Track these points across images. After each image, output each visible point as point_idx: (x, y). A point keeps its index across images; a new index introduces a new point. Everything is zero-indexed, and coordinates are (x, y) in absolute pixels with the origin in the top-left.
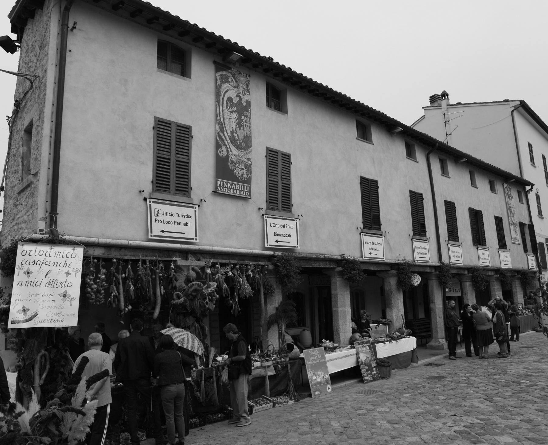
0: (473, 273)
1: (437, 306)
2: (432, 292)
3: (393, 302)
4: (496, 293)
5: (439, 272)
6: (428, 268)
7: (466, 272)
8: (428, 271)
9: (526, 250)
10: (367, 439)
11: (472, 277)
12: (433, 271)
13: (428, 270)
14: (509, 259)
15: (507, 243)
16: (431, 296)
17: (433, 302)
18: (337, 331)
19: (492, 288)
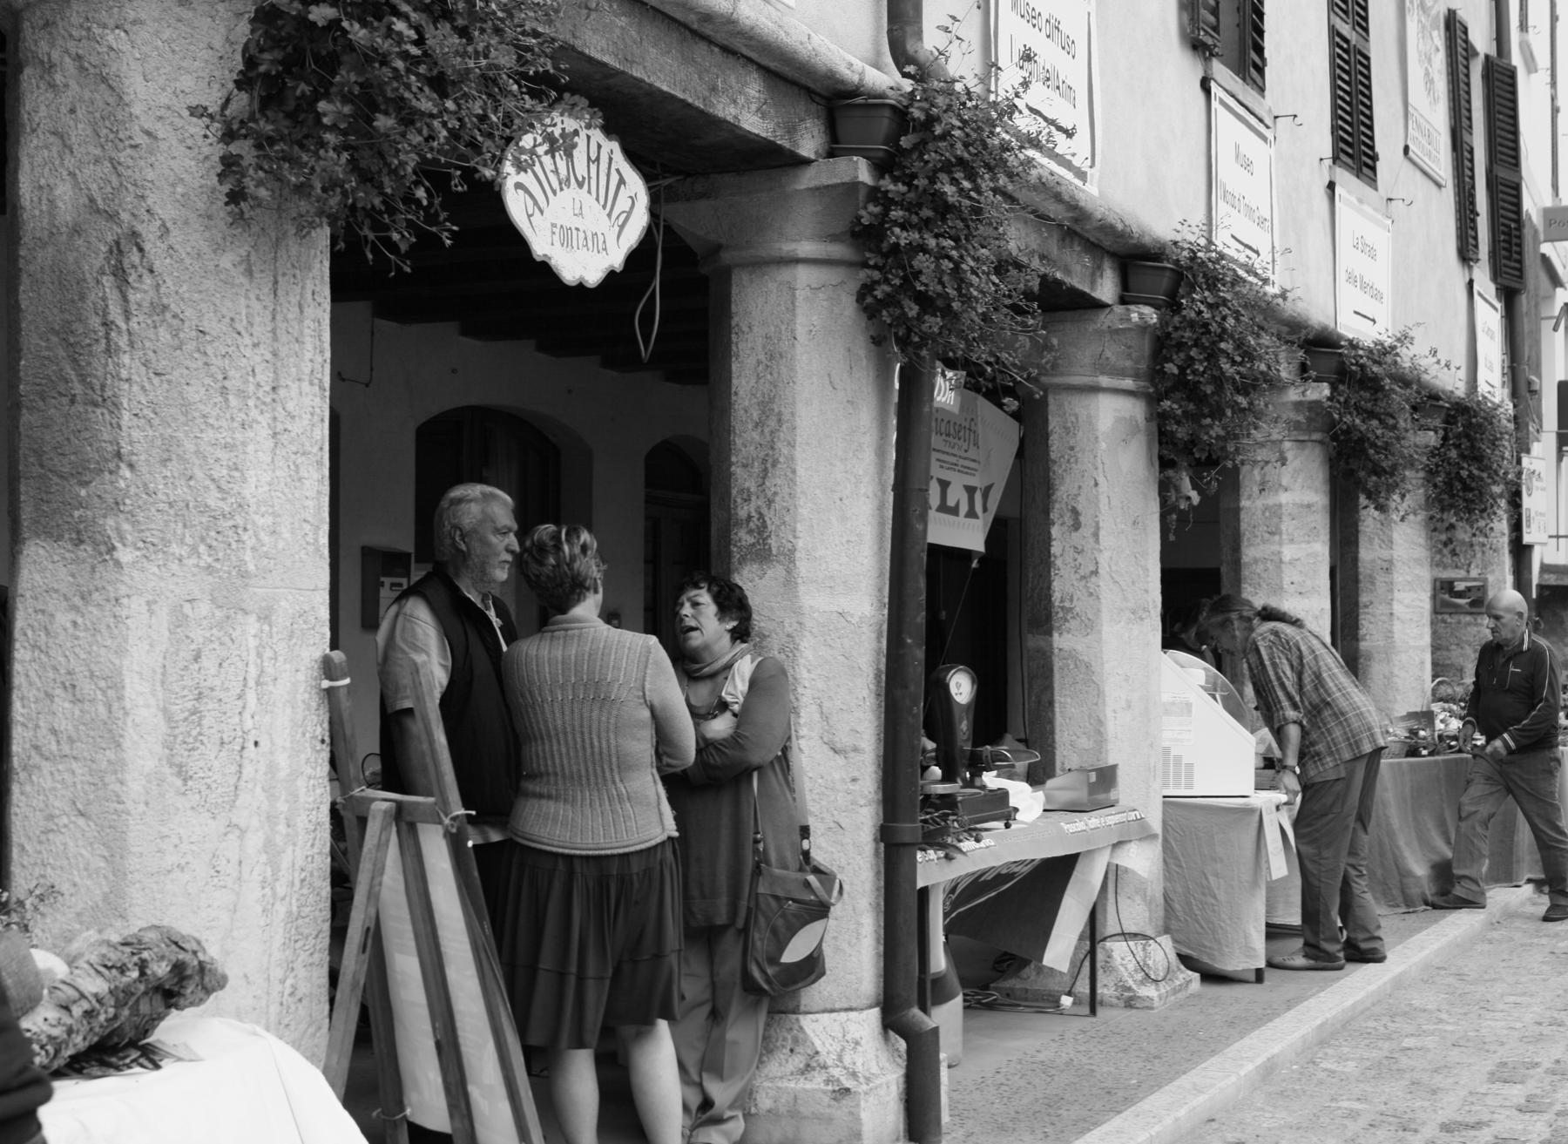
0: (1171, 305)
1: (814, 601)
2: (771, 413)
3: (134, 434)
4: (1288, 552)
5: (882, 167)
6: (754, 88)
7: (1106, 289)
8: (754, 123)
9: (1466, 254)
10: (36, 748)
11: (1162, 343)
12: (809, 143)
13: (748, 110)
14: (1380, 273)
15: (1380, 147)
16: (743, 478)
17: (762, 554)
18: (878, 941)
19: (1252, 505)
